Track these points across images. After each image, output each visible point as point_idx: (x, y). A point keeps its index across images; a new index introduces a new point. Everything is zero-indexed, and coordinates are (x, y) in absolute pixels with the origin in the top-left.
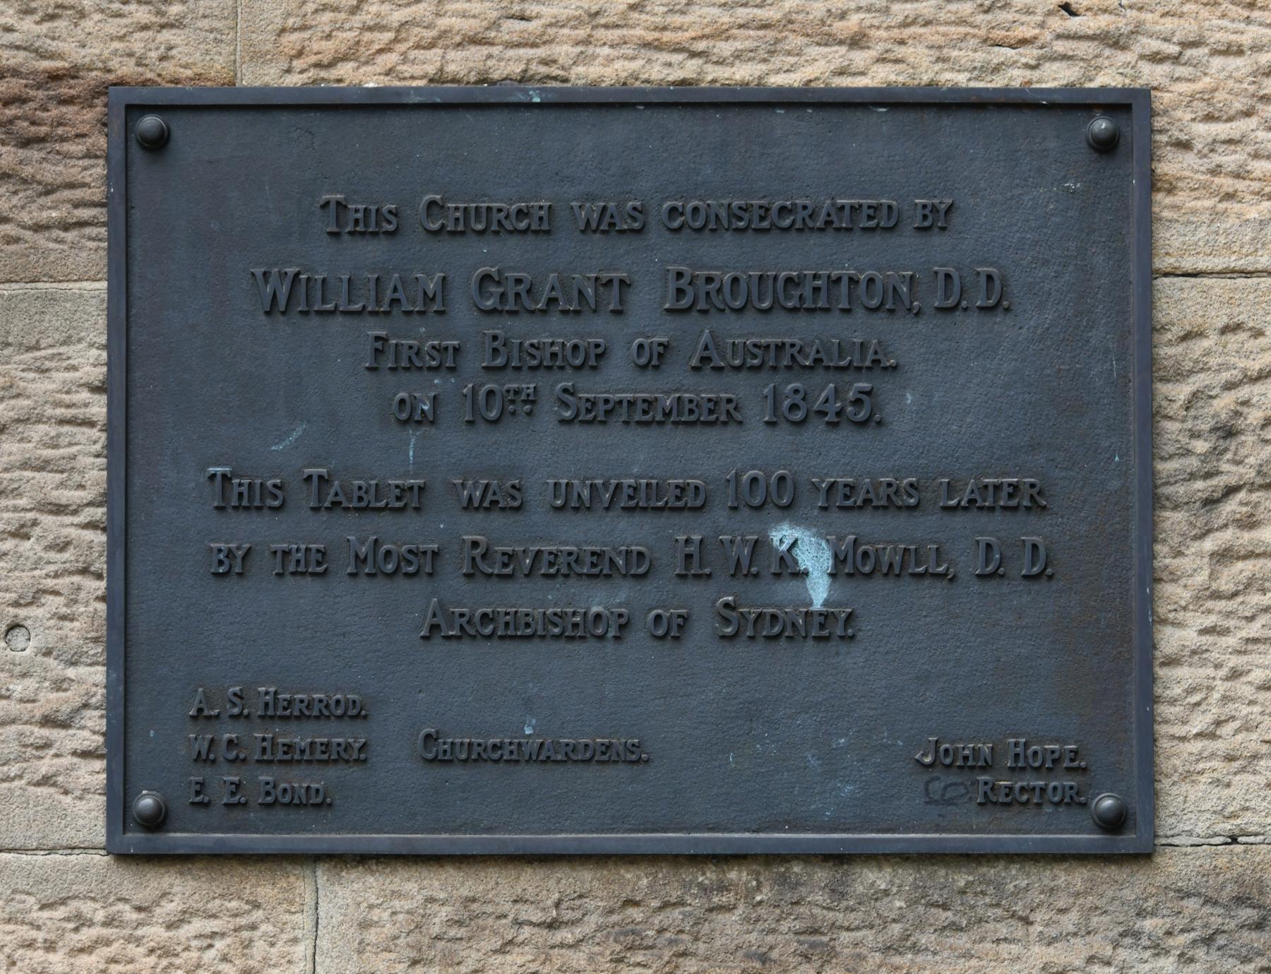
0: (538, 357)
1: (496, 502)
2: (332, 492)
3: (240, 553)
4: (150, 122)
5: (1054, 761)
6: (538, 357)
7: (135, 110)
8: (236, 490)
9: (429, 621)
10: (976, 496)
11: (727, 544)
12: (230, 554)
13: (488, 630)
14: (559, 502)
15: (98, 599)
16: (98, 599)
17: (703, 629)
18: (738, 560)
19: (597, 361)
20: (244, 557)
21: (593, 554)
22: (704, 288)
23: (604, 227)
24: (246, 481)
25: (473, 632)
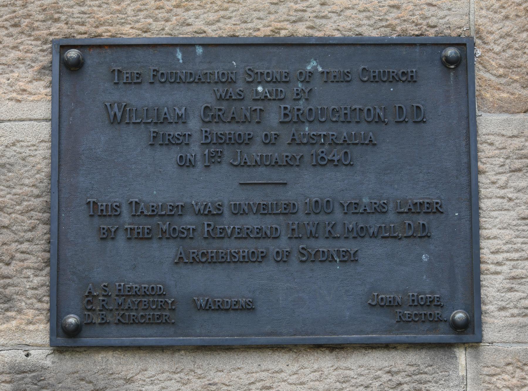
0: (243, 96)
1: (209, 212)
2: (140, 208)
3: (113, 230)
4: (73, 54)
5: (430, 302)
6: (243, 96)
7: (64, 48)
8: (100, 208)
9: (179, 256)
10: (412, 207)
11: (306, 225)
12: (109, 230)
13: (204, 260)
14: (269, 79)
15: (484, 172)
16: (484, 172)
17: (295, 258)
18: (311, 231)
19: (275, 141)
20: (115, 232)
21: (137, 73)
22: (160, 304)
23: (207, 308)
24: (104, 204)
25: (137, 322)
